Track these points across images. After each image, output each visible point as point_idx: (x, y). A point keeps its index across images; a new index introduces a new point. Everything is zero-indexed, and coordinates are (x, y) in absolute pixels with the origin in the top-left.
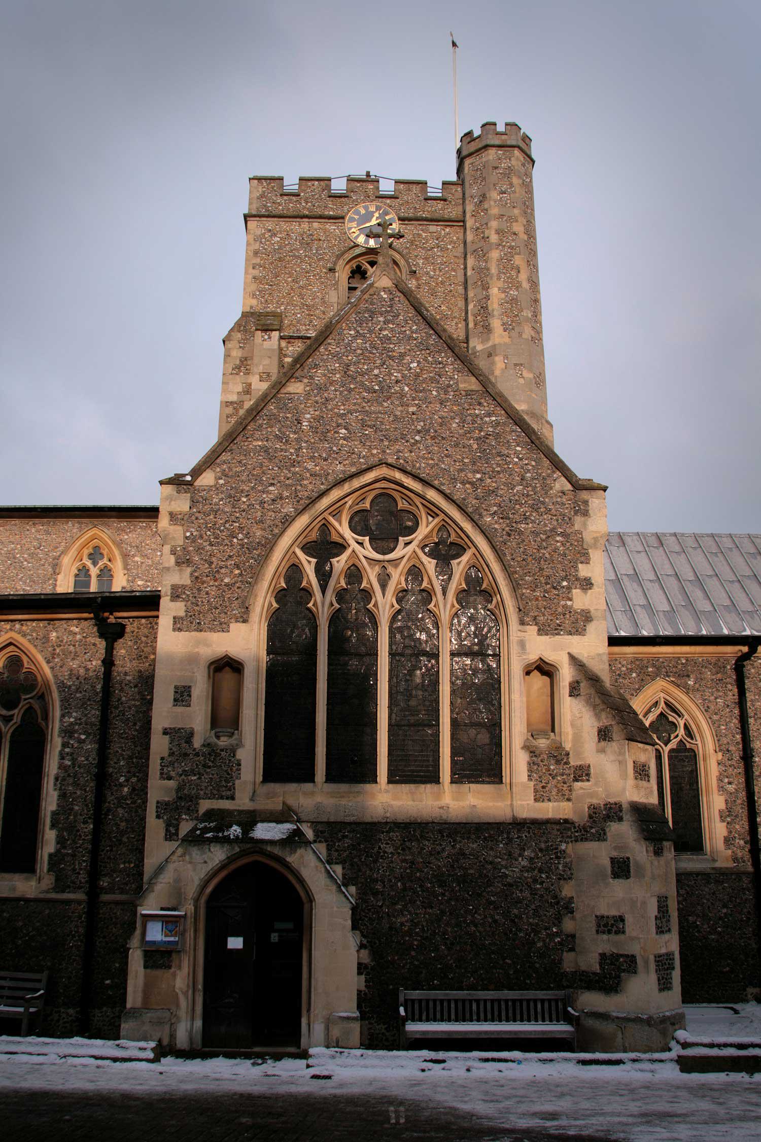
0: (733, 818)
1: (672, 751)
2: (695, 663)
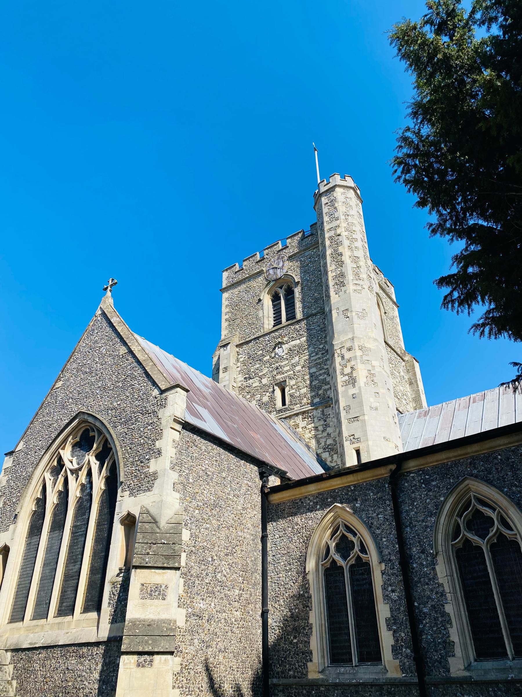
0: (398, 626)
1: (352, 566)
2: (361, 488)
